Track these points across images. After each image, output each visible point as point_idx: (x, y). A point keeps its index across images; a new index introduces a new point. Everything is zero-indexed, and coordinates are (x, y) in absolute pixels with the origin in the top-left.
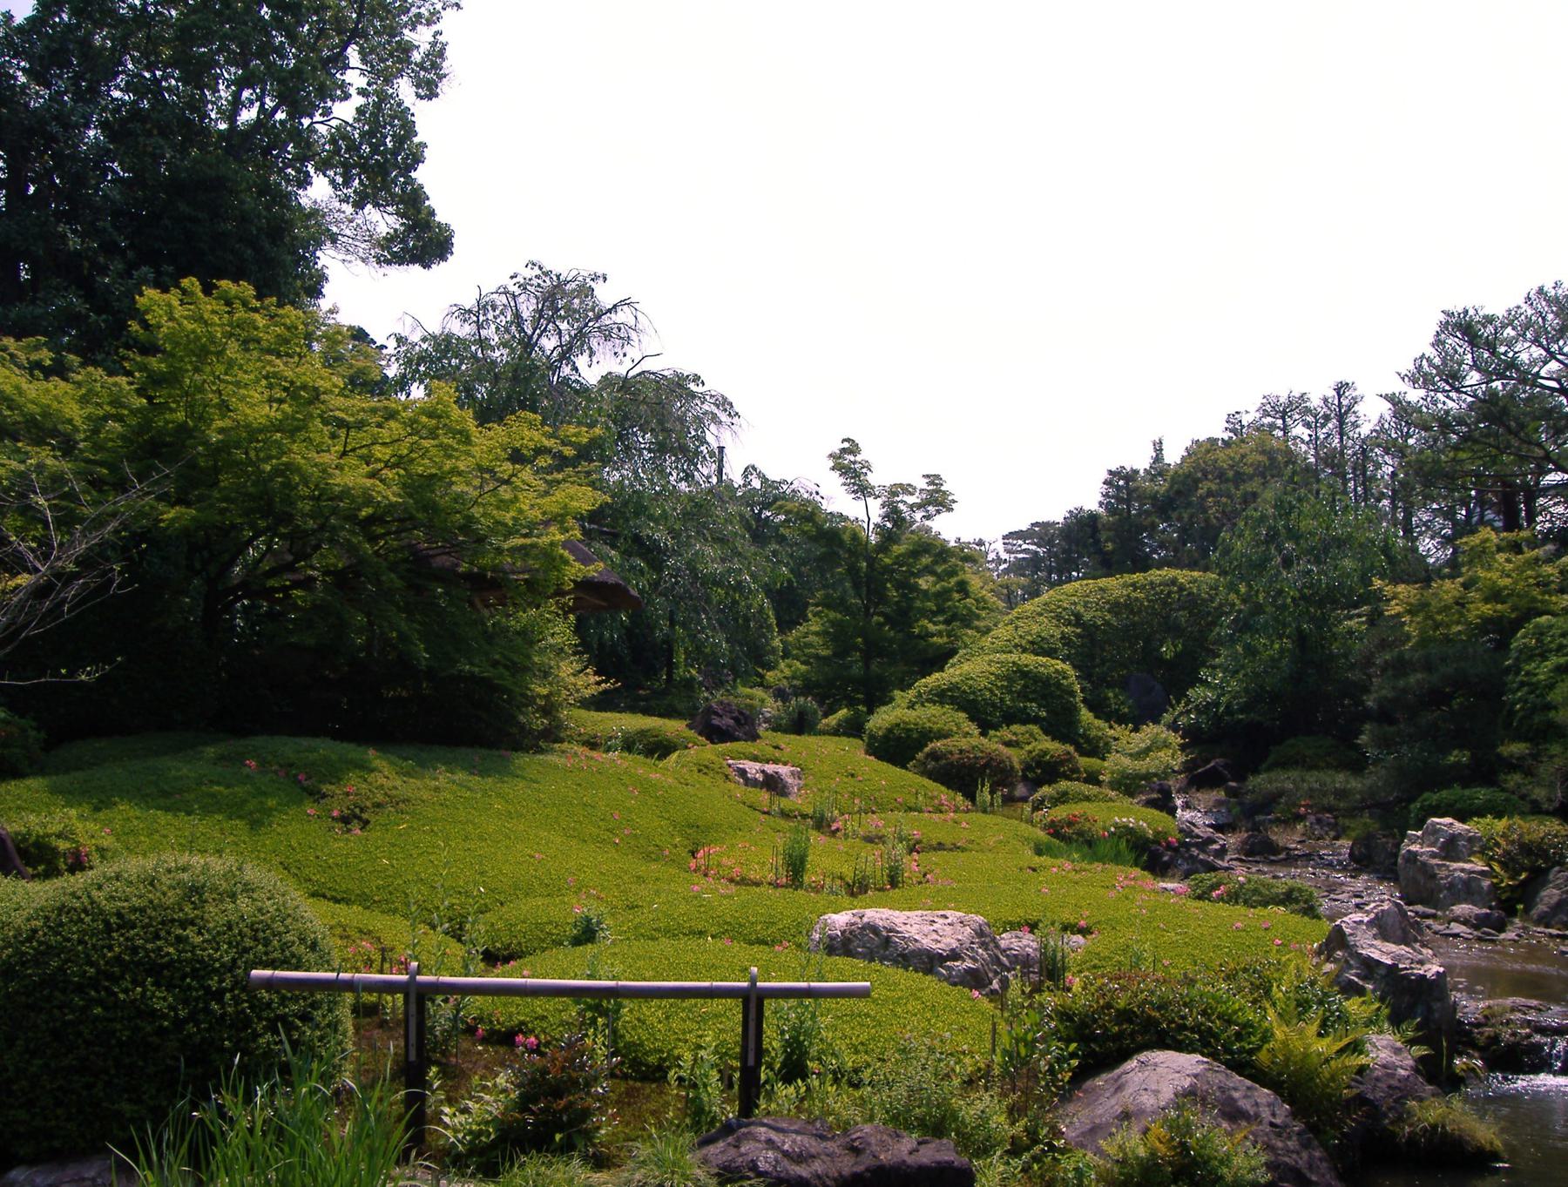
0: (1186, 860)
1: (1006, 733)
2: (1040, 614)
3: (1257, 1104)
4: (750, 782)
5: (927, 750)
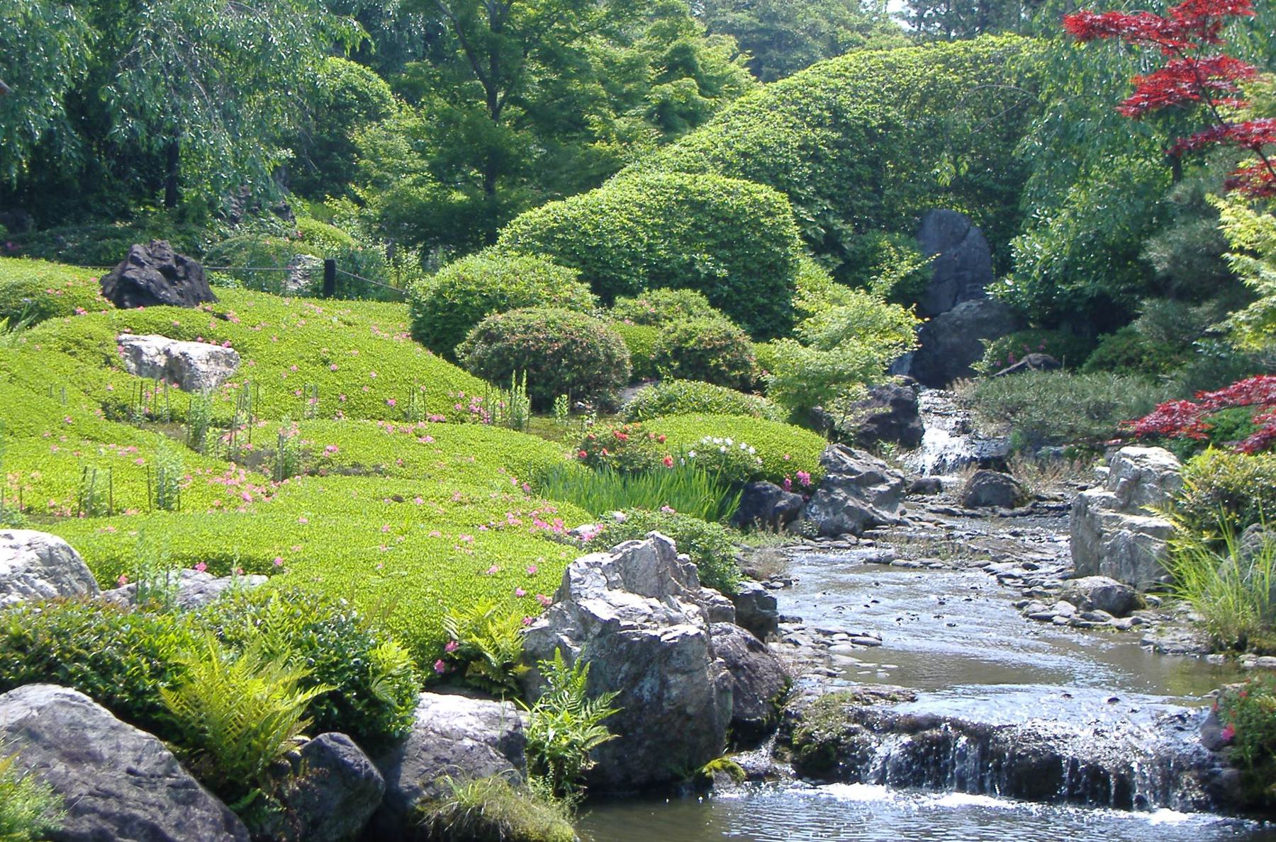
1: (644, 303)
2: (772, 107)
3: (118, 747)
5: (481, 325)
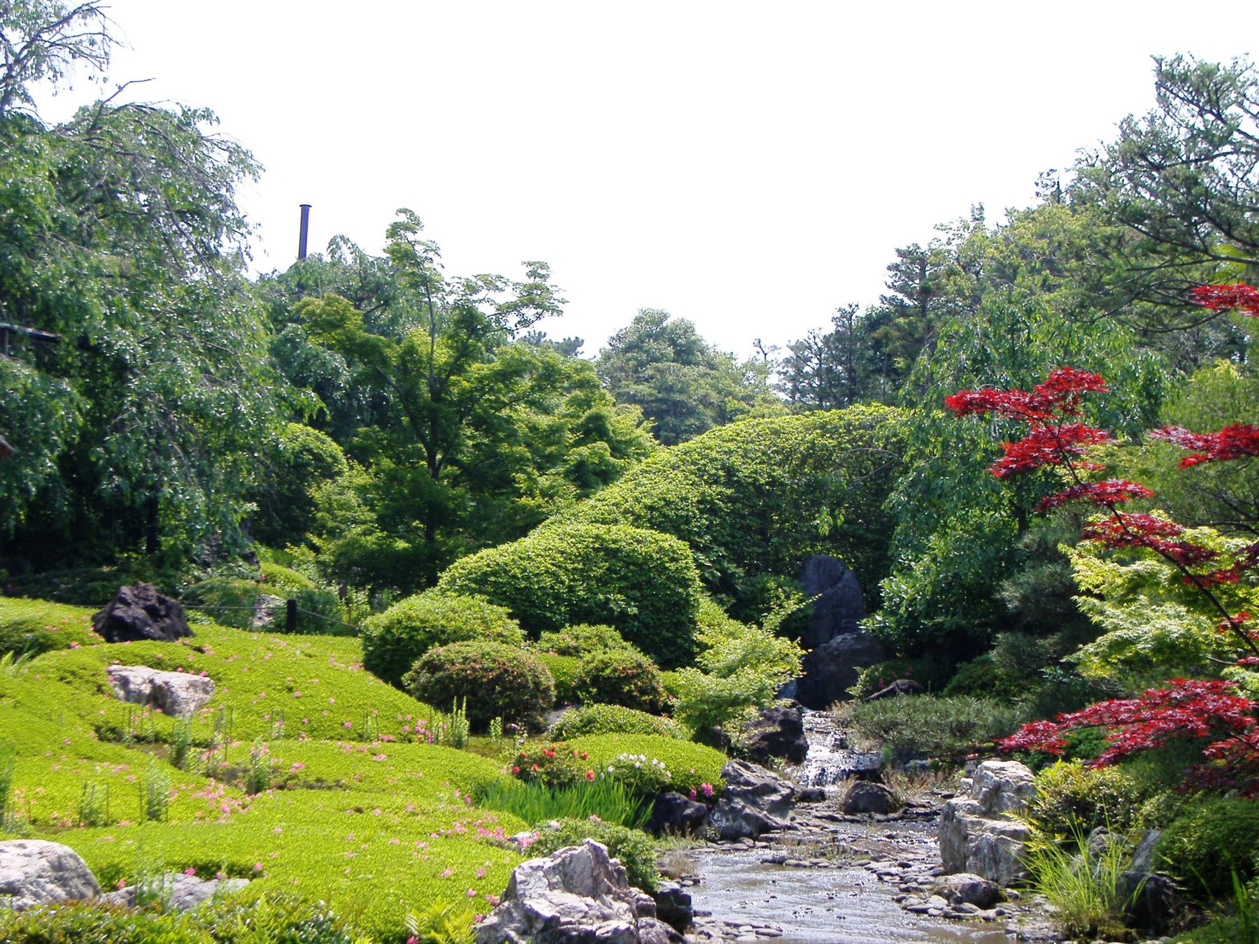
0: (724, 813)
1: (565, 637)
4: (134, 697)
5: (425, 657)
